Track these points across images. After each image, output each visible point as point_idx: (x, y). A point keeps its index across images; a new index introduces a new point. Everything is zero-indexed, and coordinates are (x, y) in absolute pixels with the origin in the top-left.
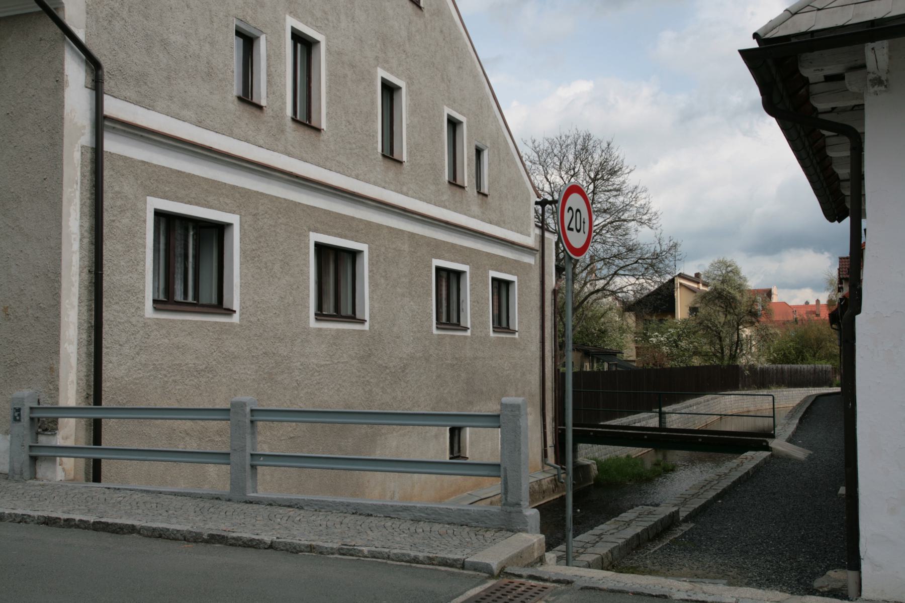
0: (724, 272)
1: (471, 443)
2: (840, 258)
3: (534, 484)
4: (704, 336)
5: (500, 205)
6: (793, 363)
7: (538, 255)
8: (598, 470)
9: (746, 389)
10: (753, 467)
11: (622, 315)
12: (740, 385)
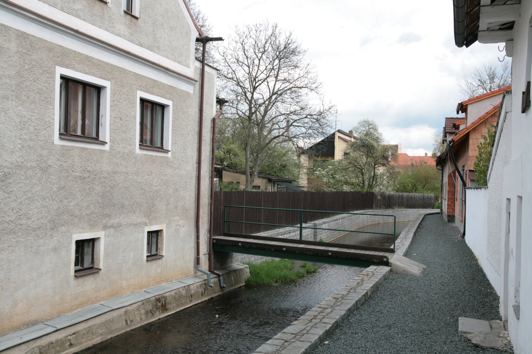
0: (367, 128)
1: (107, 255)
2: (446, 118)
3: (181, 290)
4: (353, 172)
5: (154, 31)
6: (410, 192)
7: (198, 85)
8: (250, 273)
9: (378, 208)
10: (373, 287)
11: (299, 156)
12: (374, 206)
